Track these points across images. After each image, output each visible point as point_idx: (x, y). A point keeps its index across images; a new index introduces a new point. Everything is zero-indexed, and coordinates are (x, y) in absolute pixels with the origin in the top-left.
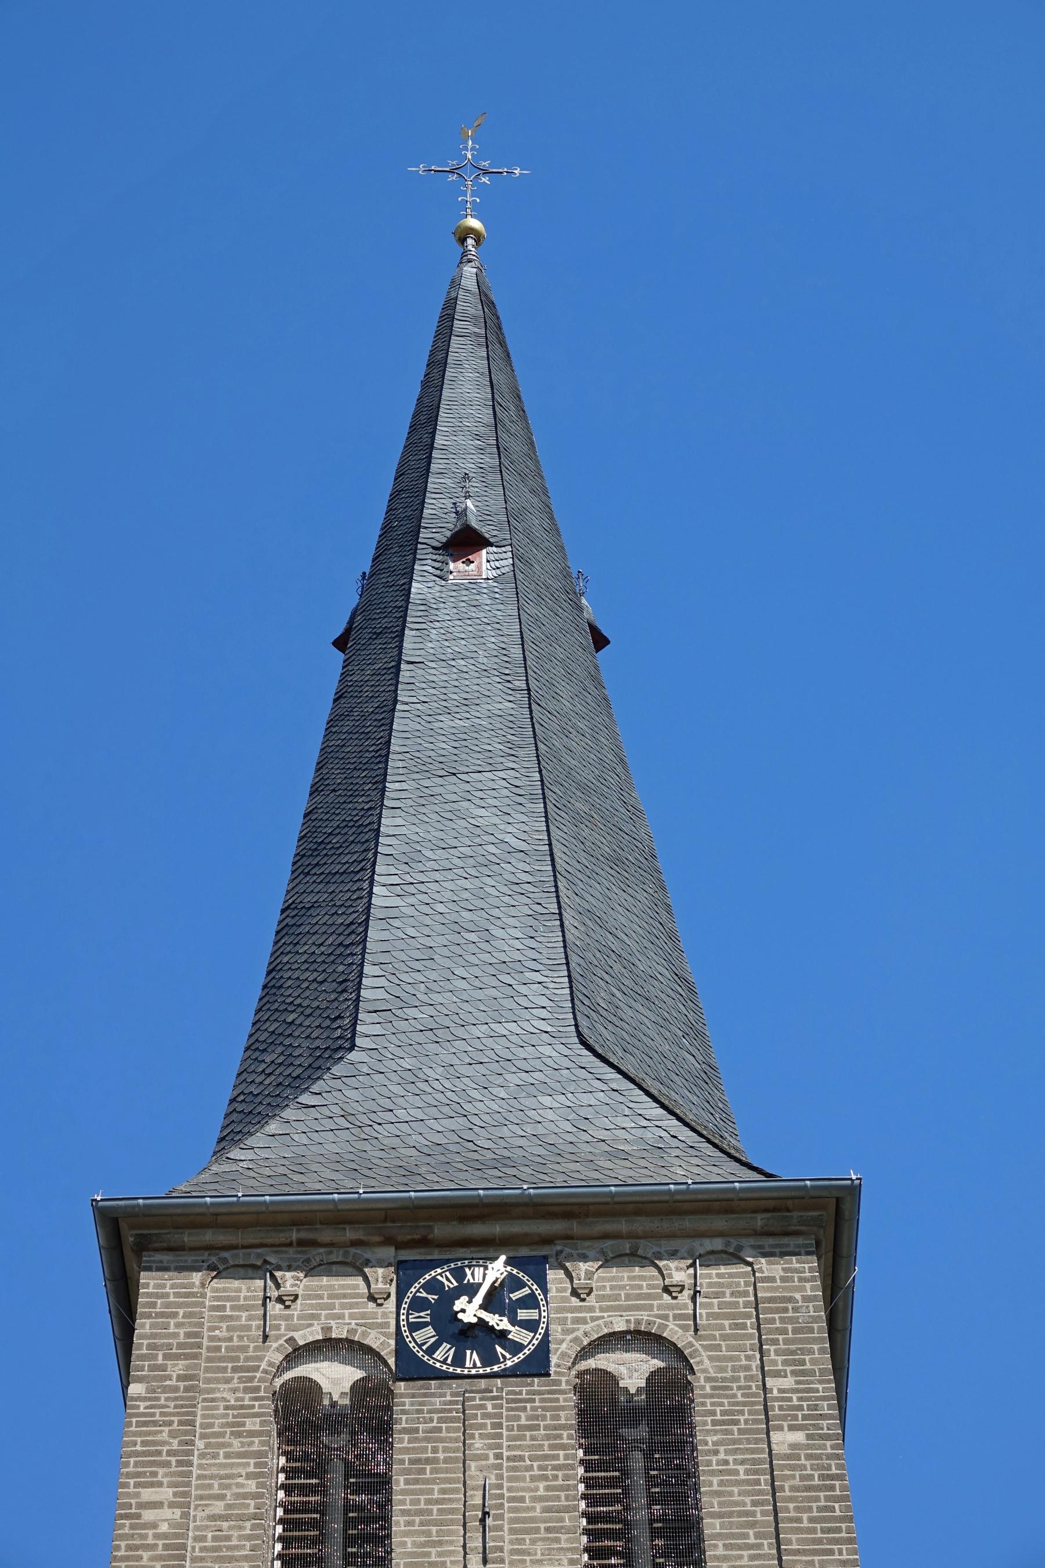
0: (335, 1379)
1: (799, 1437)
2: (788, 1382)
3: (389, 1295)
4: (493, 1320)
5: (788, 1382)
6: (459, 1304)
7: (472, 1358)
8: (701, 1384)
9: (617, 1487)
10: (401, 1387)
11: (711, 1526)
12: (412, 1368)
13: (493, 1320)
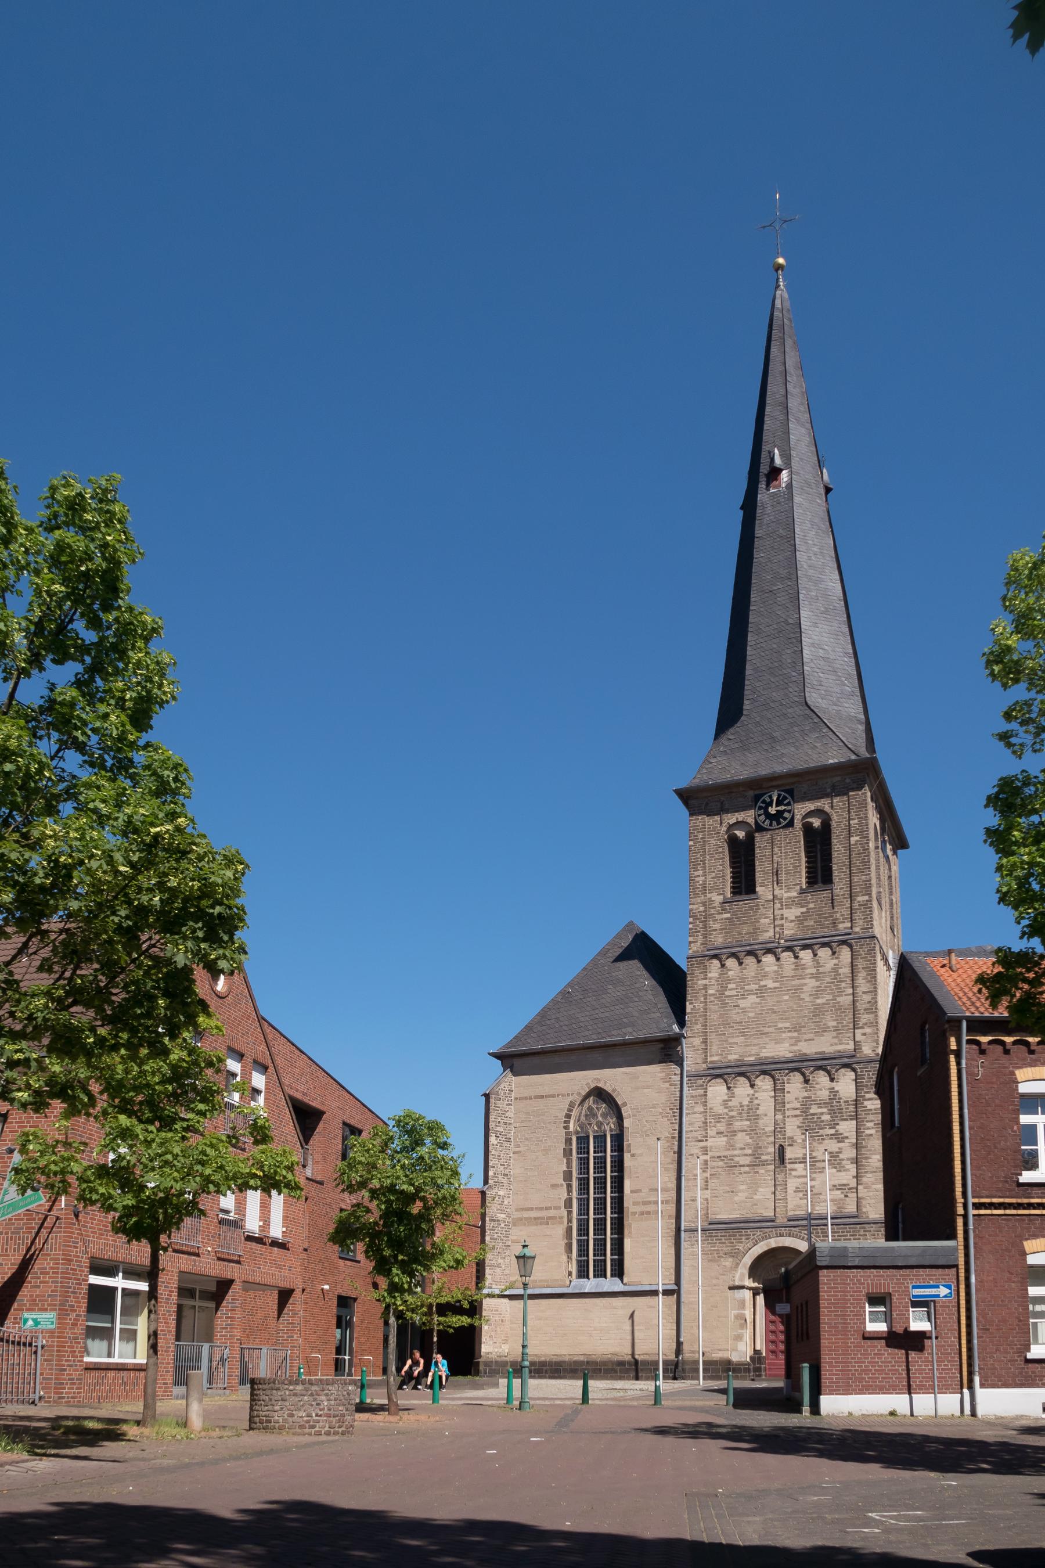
0: (741, 834)
1: (858, 838)
2: (856, 821)
3: (600, 1094)
4: (779, 808)
5: (856, 821)
6: (770, 809)
7: (774, 823)
8: (834, 824)
9: (56, 1540)
10: (757, 834)
11: (835, 867)
12: (759, 828)
13: (779, 808)
